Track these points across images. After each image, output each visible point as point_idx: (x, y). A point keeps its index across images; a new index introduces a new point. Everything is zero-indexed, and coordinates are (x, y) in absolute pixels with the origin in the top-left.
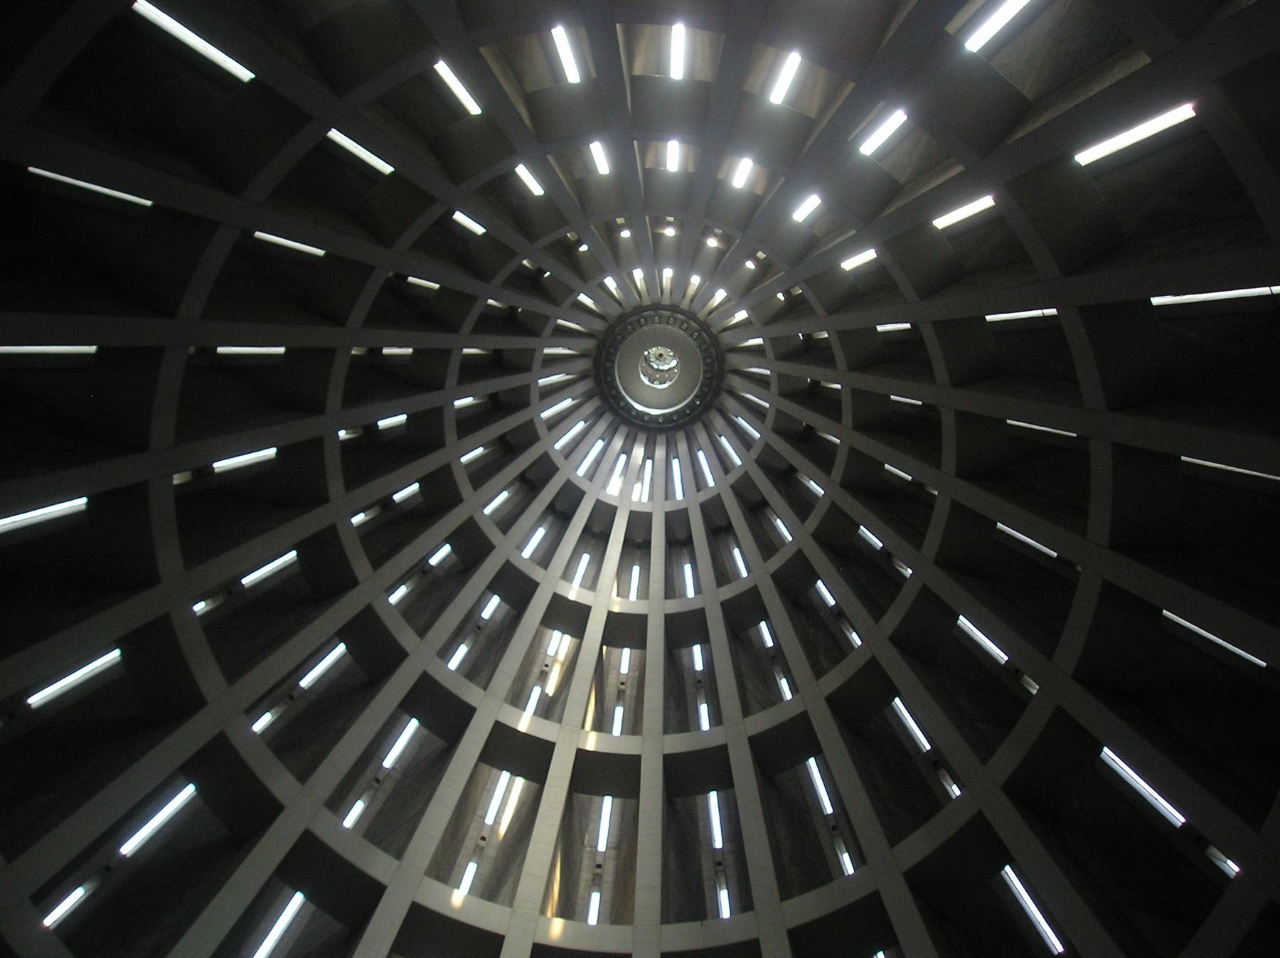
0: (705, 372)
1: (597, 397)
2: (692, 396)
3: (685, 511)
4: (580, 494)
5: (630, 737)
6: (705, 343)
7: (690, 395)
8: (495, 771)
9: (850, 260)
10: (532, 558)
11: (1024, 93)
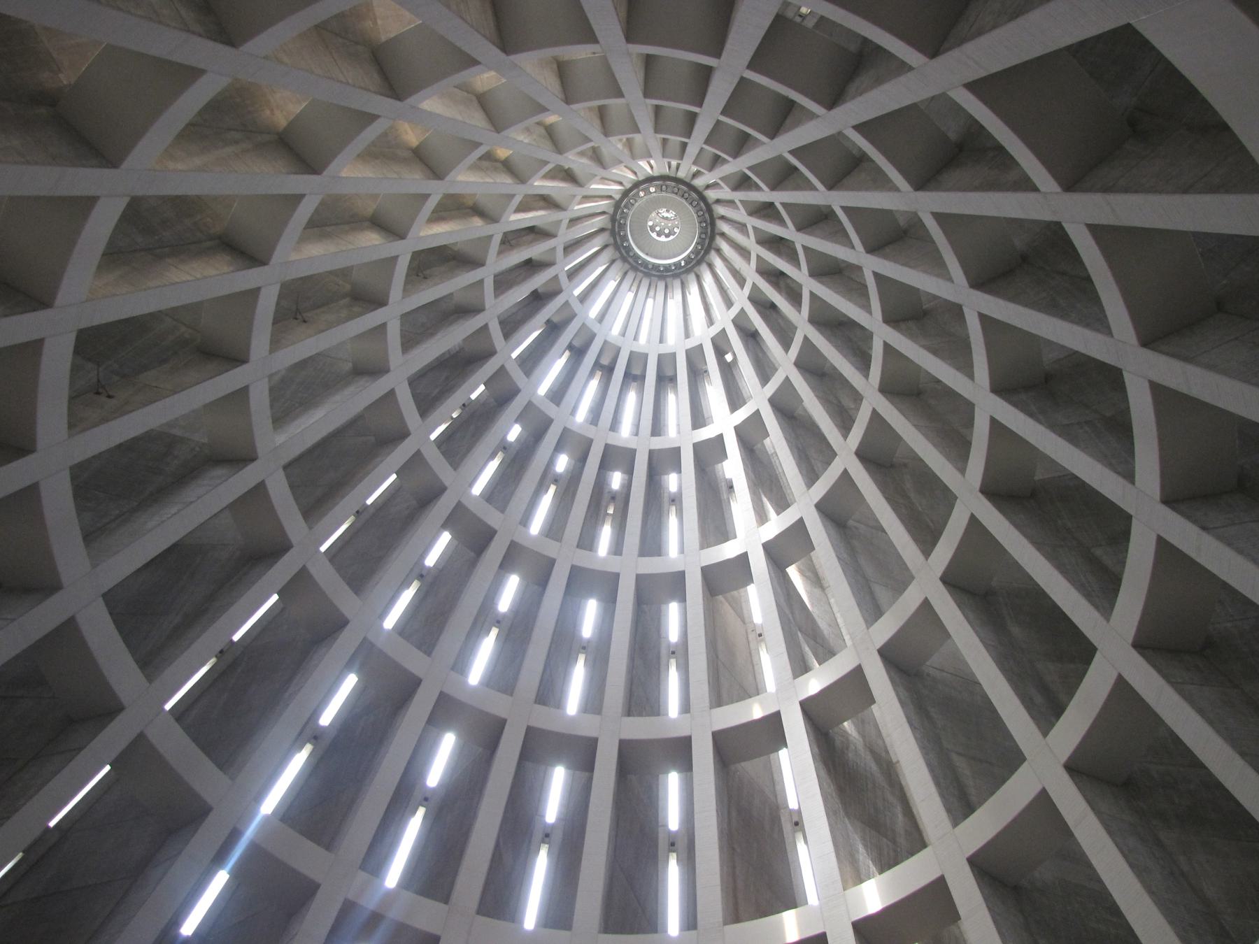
0: (701, 234)
1: (612, 246)
2: (694, 244)
3: (674, 355)
4: (592, 337)
5: (172, 720)
6: (702, 210)
7: (687, 250)
8: (742, 590)
9: (516, 585)
10: (547, 396)
11: (854, 152)
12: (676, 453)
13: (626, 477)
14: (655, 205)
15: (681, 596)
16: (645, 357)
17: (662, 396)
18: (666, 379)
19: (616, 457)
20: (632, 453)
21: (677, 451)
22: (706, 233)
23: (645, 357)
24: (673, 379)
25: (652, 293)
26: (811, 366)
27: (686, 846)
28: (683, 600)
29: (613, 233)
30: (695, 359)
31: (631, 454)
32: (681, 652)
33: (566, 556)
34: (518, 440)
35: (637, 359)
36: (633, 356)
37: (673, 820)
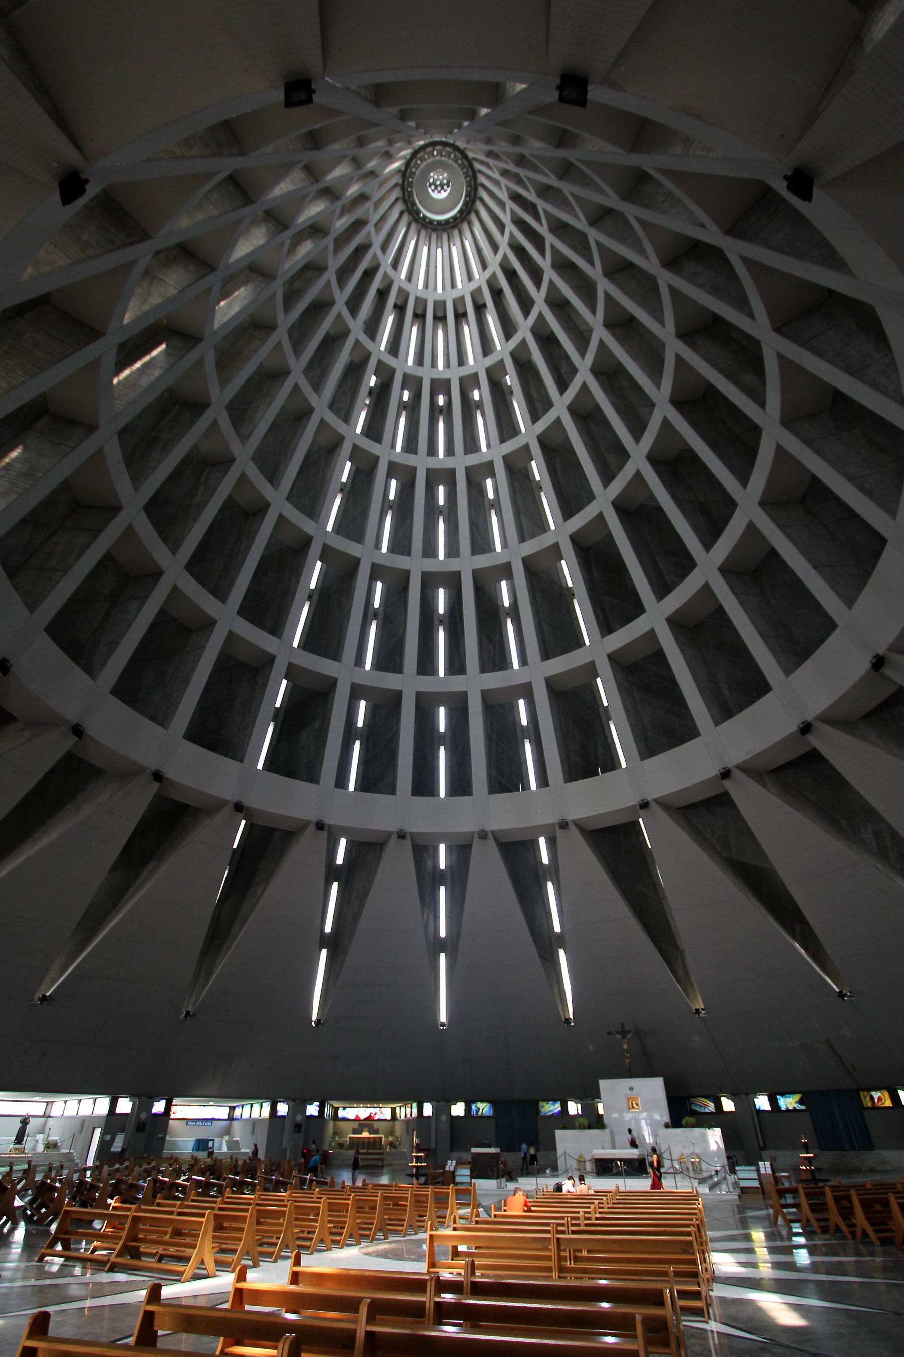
0: (467, 187)
12: (475, 376)
13: (447, 398)
14: (434, 167)
15: (493, 476)
16: (444, 303)
17: (459, 329)
18: (460, 316)
19: (441, 385)
20: (448, 382)
21: (490, 464)
22: (470, 186)
23: (444, 303)
24: (465, 314)
25: (440, 244)
26: (558, 304)
27: (514, 612)
28: (479, 388)
29: (405, 201)
30: (476, 295)
31: (448, 382)
32: (495, 504)
33: (421, 463)
34: (375, 385)
35: (440, 305)
36: (436, 303)
37: (491, 495)
